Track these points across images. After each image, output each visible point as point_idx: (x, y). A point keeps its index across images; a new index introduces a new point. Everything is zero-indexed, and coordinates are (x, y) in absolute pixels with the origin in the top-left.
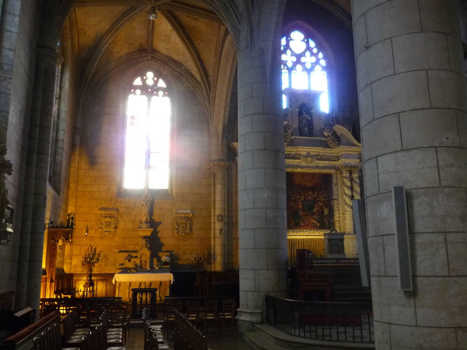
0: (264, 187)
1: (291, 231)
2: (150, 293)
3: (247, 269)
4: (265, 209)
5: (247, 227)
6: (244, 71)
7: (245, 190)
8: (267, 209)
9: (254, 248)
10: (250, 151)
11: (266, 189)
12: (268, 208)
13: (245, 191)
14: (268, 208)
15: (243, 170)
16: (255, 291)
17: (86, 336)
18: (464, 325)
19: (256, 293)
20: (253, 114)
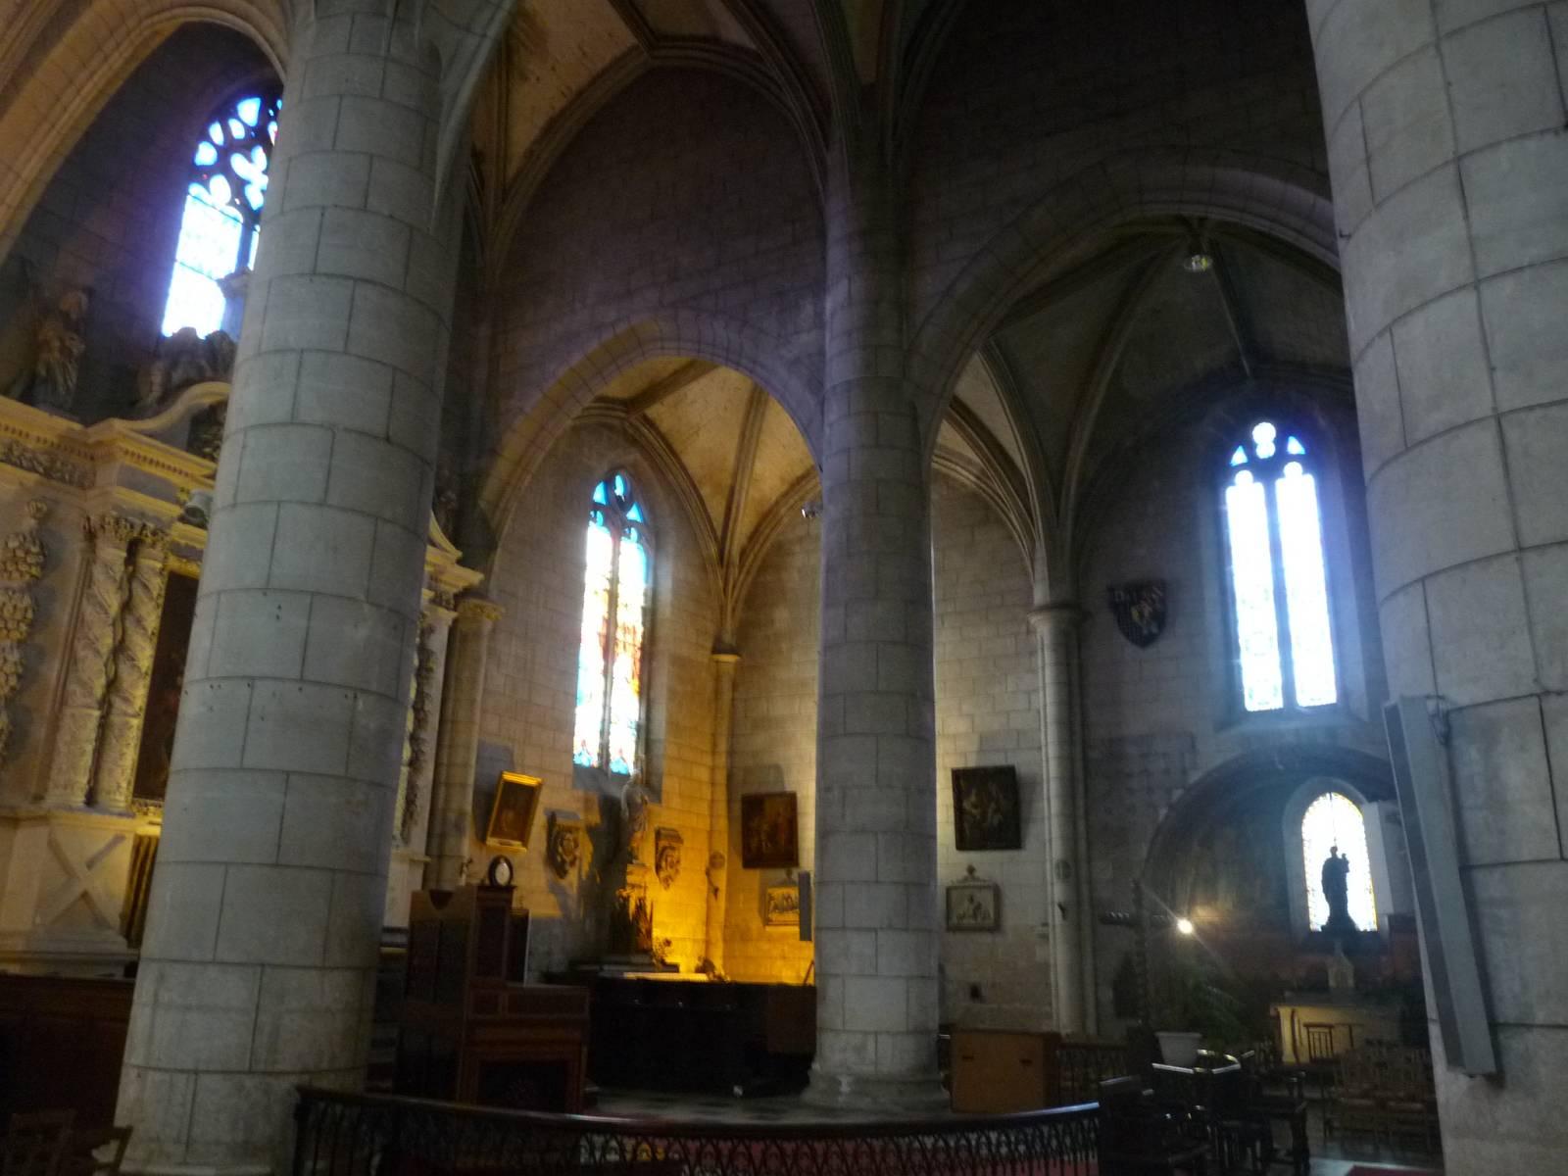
0: (362, 597)
1: (152, 805)
2: (1319, 913)
3: (213, 962)
4: (351, 694)
5: (249, 762)
6: (341, 97)
7: (265, 591)
8: (359, 695)
9: (276, 865)
10: (321, 426)
11: (366, 608)
12: (364, 691)
13: (265, 594)
14: (364, 691)
15: (266, 502)
16: (250, 1072)
17: (1140, 1022)
18: (1562, 1021)
19: (249, 1082)
20: (357, 280)
